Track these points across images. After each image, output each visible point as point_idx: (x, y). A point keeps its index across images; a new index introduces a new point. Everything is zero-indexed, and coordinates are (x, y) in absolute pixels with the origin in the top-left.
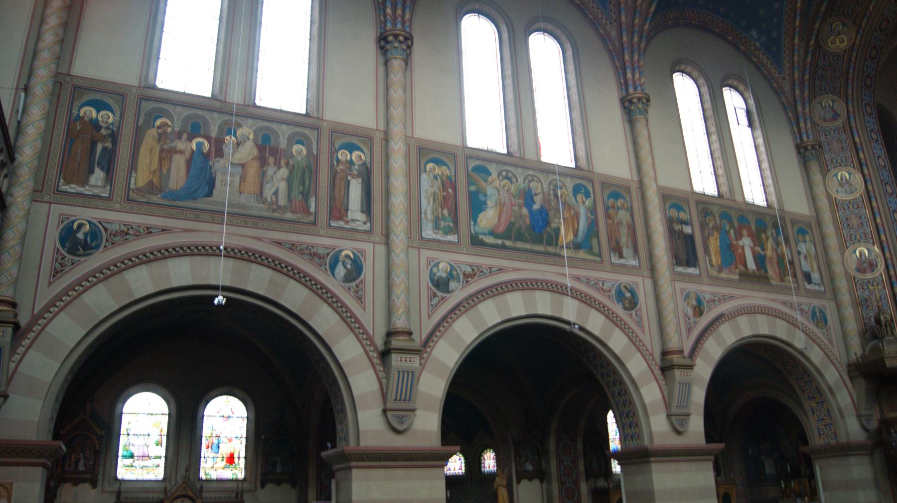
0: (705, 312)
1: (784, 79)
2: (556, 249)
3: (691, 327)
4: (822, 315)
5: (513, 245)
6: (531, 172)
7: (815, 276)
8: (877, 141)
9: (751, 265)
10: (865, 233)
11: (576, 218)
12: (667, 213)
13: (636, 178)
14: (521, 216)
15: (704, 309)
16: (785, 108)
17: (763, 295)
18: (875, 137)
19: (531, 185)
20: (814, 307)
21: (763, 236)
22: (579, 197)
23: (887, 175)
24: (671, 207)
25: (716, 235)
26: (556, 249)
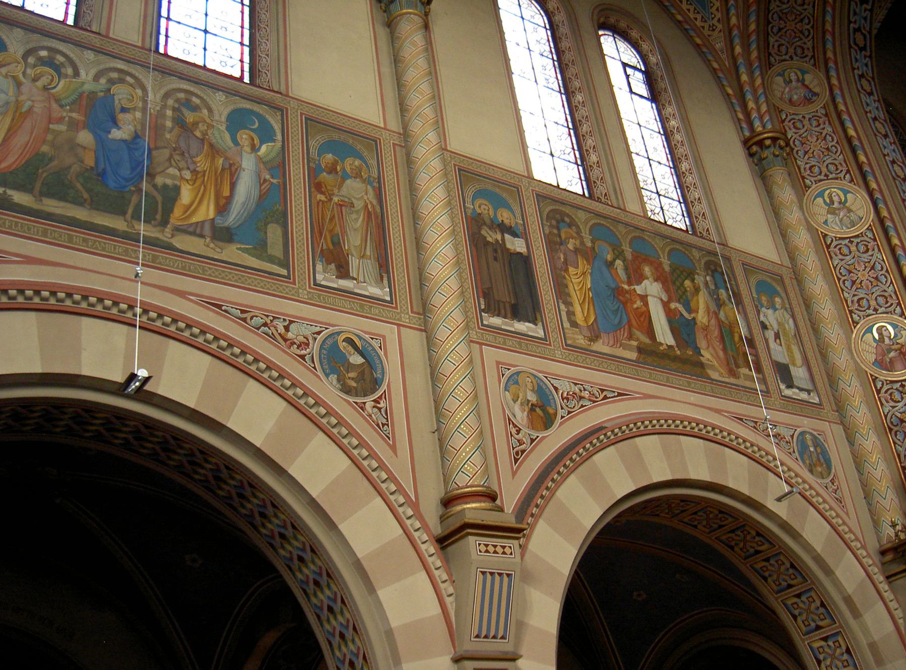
0: (558, 420)
1: (713, 30)
2: (163, 231)
3: (523, 451)
4: (819, 450)
5: (36, 206)
6: (121, 65)
7: (799, 373)
8: (886, 136)
9: (665, 336)
10: (803, 49)
11: (227, 175)
12: (469, 205)
13: (394, 125)
14: (73, 146)
15: (556, 414)
16: (718, 80)
17: (693, 398)
18: (867, 88)
19: (114, 89)
20: (803, 433)
21: (687, 283)
22: (244, 137)
23: (891, 149)
24: (479, 194)
25: (582, 264)
26: (163, 231)
